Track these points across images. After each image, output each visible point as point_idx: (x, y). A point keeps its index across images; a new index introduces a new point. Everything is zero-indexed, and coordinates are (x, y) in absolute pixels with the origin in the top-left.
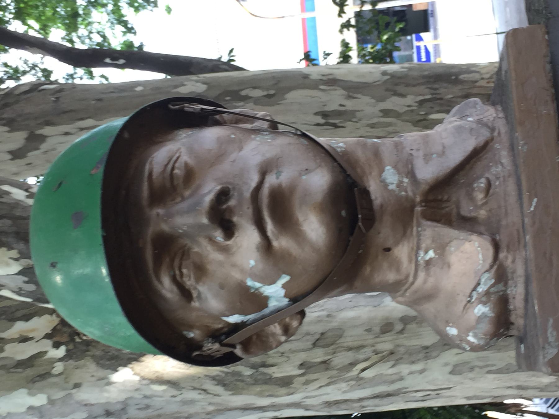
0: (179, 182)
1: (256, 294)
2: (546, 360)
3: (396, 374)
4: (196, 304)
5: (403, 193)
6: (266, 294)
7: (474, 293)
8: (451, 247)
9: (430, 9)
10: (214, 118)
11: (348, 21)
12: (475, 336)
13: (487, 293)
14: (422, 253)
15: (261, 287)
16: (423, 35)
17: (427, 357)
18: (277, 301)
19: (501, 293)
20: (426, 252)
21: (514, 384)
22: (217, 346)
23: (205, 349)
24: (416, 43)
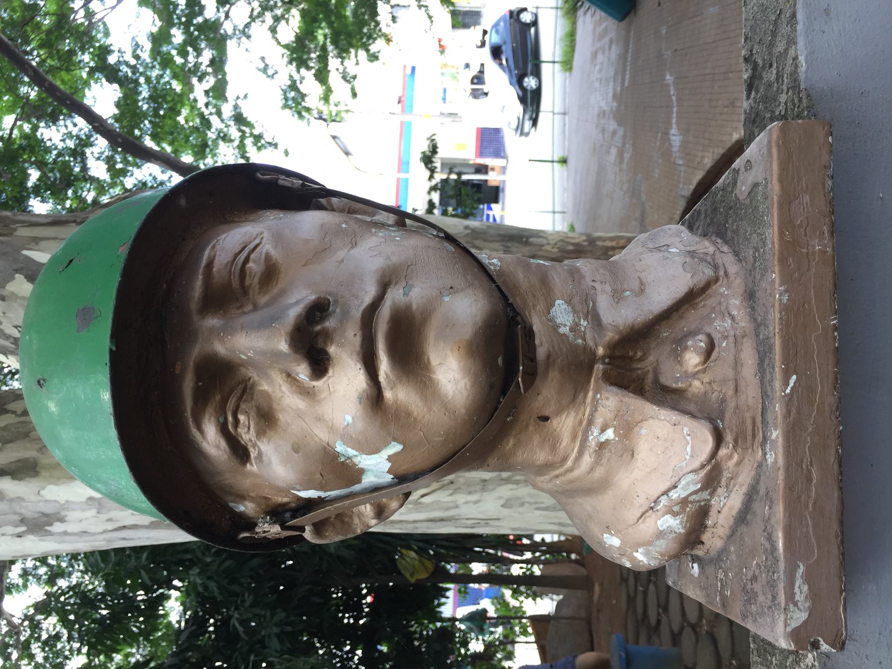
0: (253, 282)
1: (347, 465)
2: (789, 629)
3: (452, 502)
4: (252, 467)
5: (580, 341)
6: (361, 466)
7: (665, 497)
8: (641, 428)
9: (501, 186)
10: (319, 202)
11: (436, 185)
12: (646, 554)
13: (684, 502)
14: (596, 431)
15: (356, 456)
16: (493, 206)
17: (483, 490)
18: (376, 476)
19: (702, 504)
20: (603, 430)
21: (556, 521)
22: (276, 529)
23: (258, 530)
24: (486, 212)
